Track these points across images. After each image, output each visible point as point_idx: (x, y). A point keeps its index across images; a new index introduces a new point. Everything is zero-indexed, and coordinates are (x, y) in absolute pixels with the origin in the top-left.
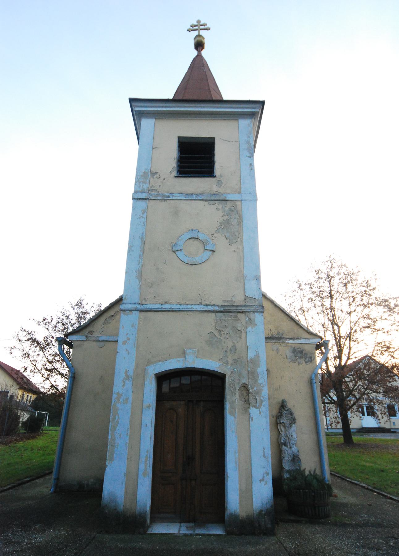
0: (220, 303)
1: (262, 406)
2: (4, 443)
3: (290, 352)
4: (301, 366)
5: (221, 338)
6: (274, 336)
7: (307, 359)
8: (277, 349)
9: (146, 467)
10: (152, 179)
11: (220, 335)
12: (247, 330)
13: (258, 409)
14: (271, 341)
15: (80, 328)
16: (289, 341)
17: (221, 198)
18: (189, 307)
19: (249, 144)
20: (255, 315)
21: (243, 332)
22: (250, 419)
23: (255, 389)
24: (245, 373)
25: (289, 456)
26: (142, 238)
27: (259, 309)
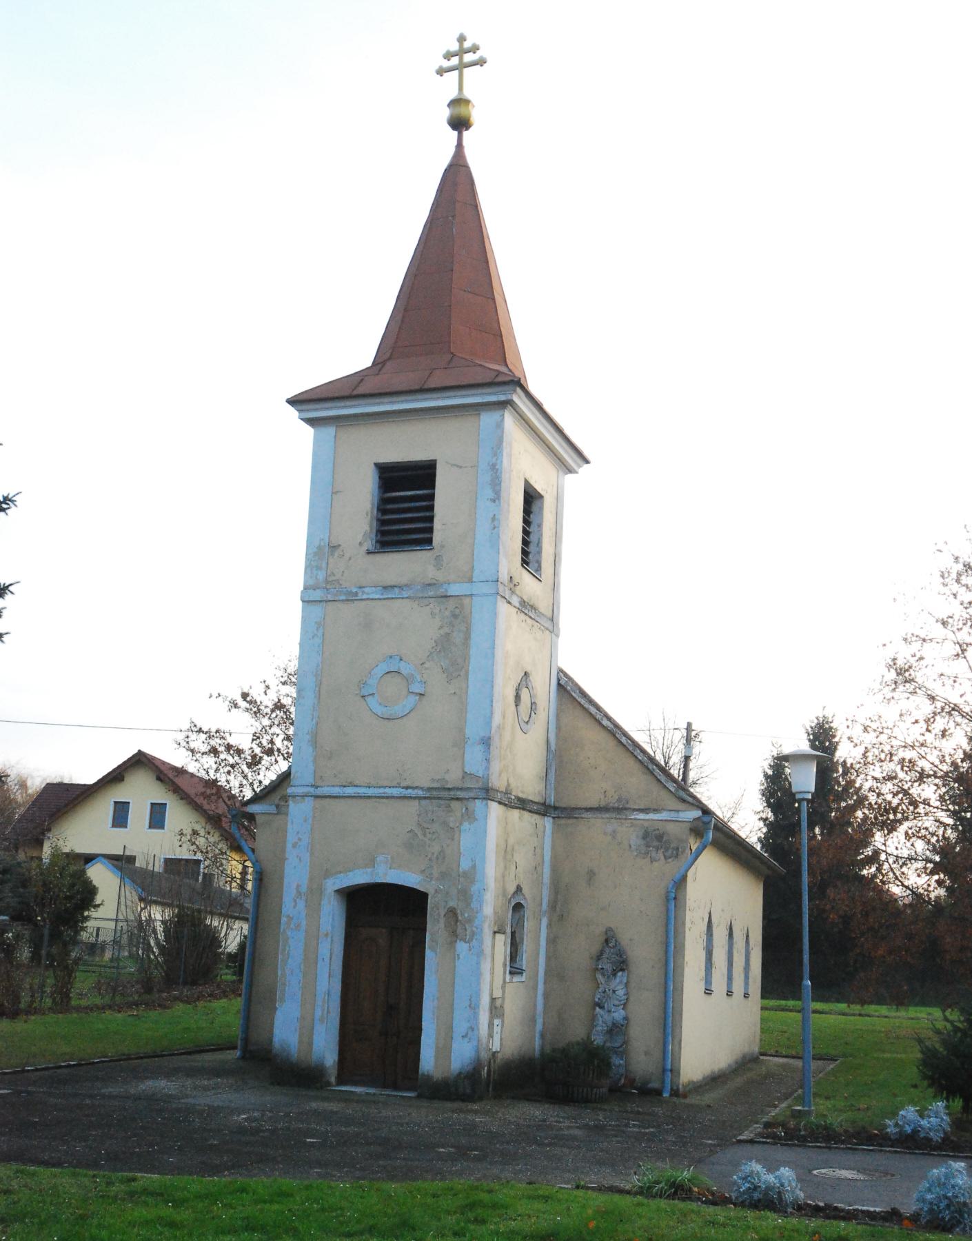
0: (427, 784)
1: (474, 940)
2: (186, 999)
3: (637, 837)
4: (656, 864)
5: (425, 839)
6: (611, 805)
7: (670, 851)
8: (614, 832)
9: (323, 1014)
10: (331, 560)
11: (425, 835)
12: (462, 828)
13: (468, 944)
14: (604, 816)
15: (266, 790)
16: (637, 814)
17: (439, 593)
18: (381, 790)
19: (495, 471)
20: (475, 803)
21: (456, 829)
22: (455, 957)
23: (466, 915)
24: (454, 892)
25: (604, 1025)
26: (316, 675)
27: (482, 795)
